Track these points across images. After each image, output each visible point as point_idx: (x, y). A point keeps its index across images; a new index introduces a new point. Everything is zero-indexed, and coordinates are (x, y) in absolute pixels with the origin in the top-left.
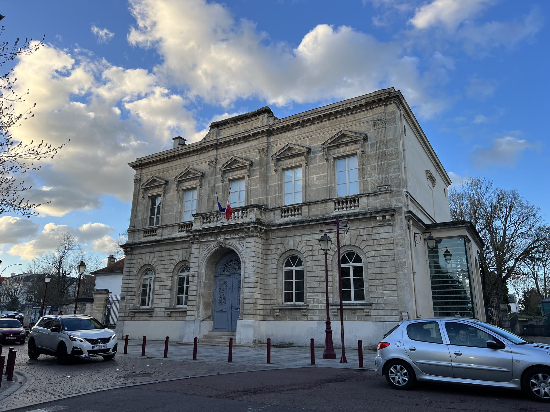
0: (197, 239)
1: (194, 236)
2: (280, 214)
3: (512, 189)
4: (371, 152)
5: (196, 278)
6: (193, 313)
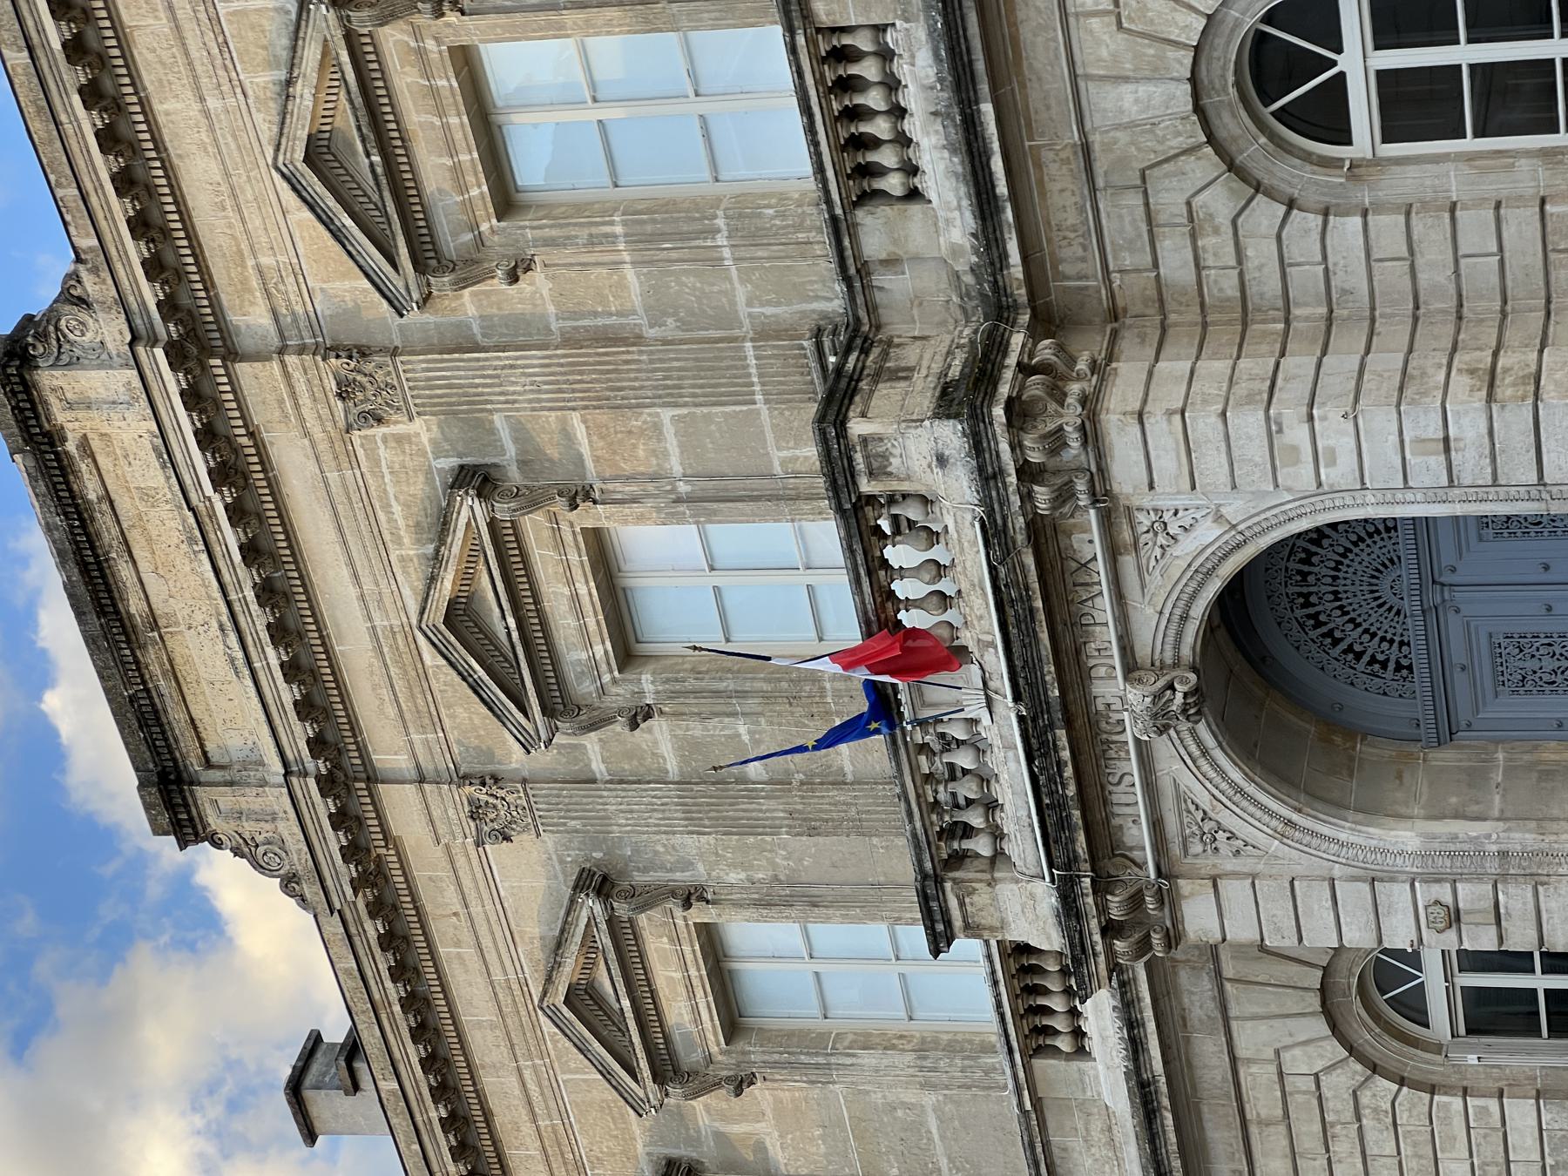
0: (1136, 901)
1: (1110, 930)
2: (885, 211)
3: (1095, 1054)
5: (1471, 895)
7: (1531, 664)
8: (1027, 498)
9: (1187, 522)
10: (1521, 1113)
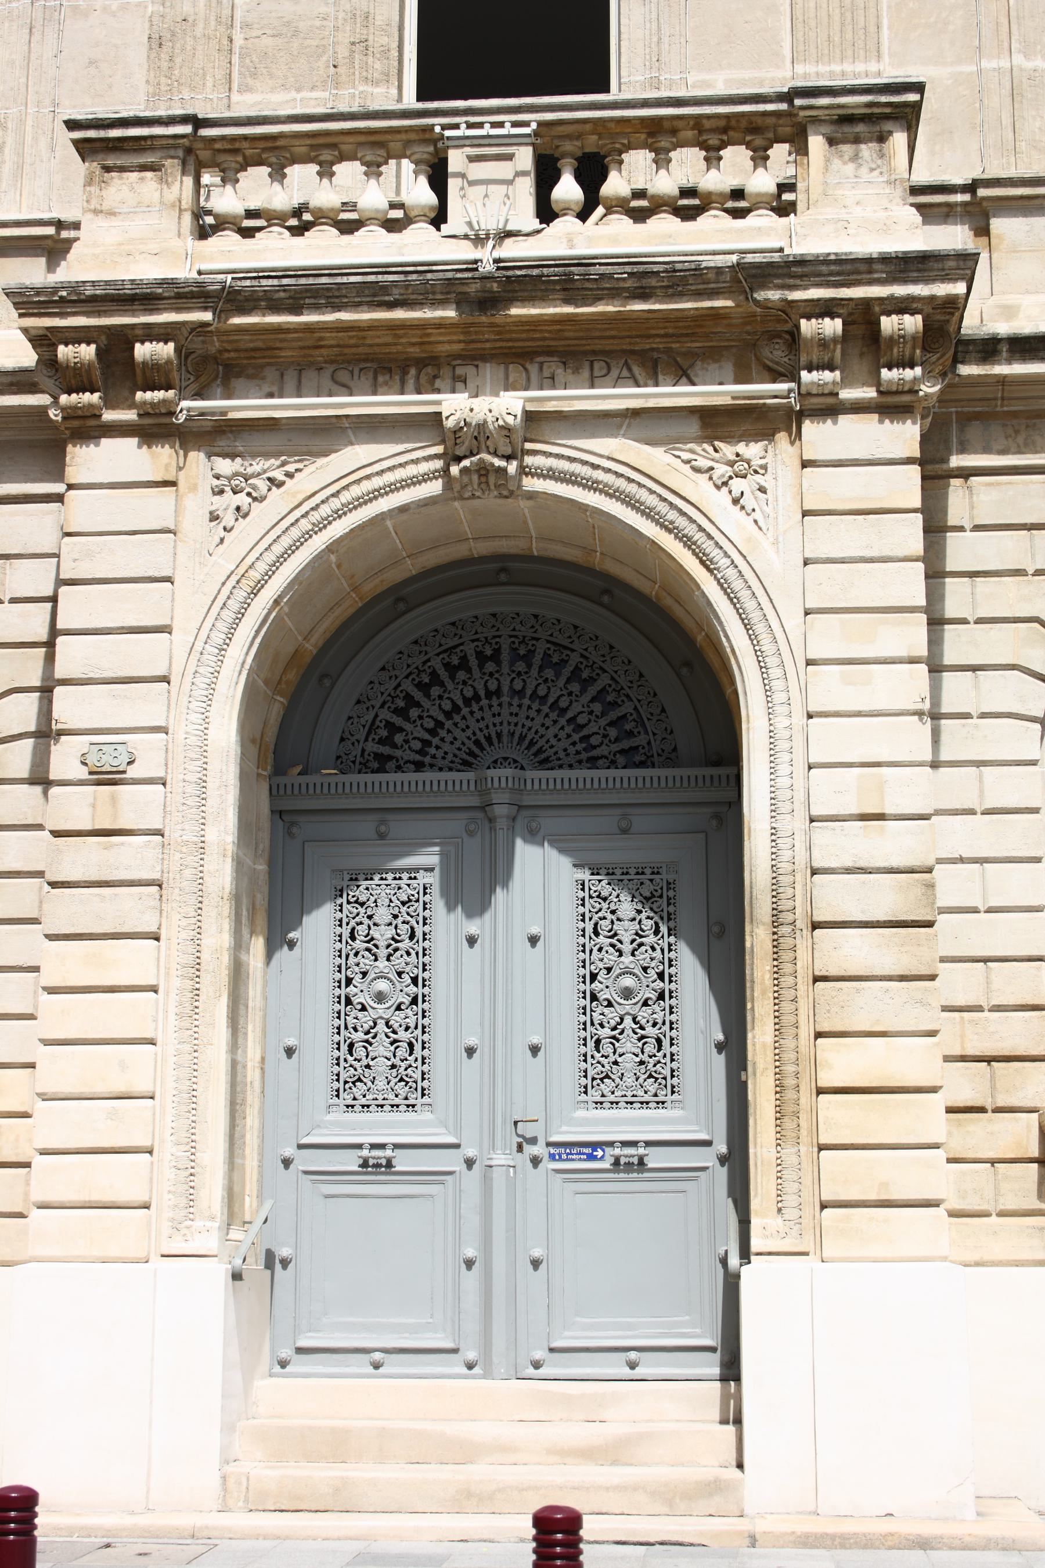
7: (383, 915)
8: (825, 309)
9: (748, 501)
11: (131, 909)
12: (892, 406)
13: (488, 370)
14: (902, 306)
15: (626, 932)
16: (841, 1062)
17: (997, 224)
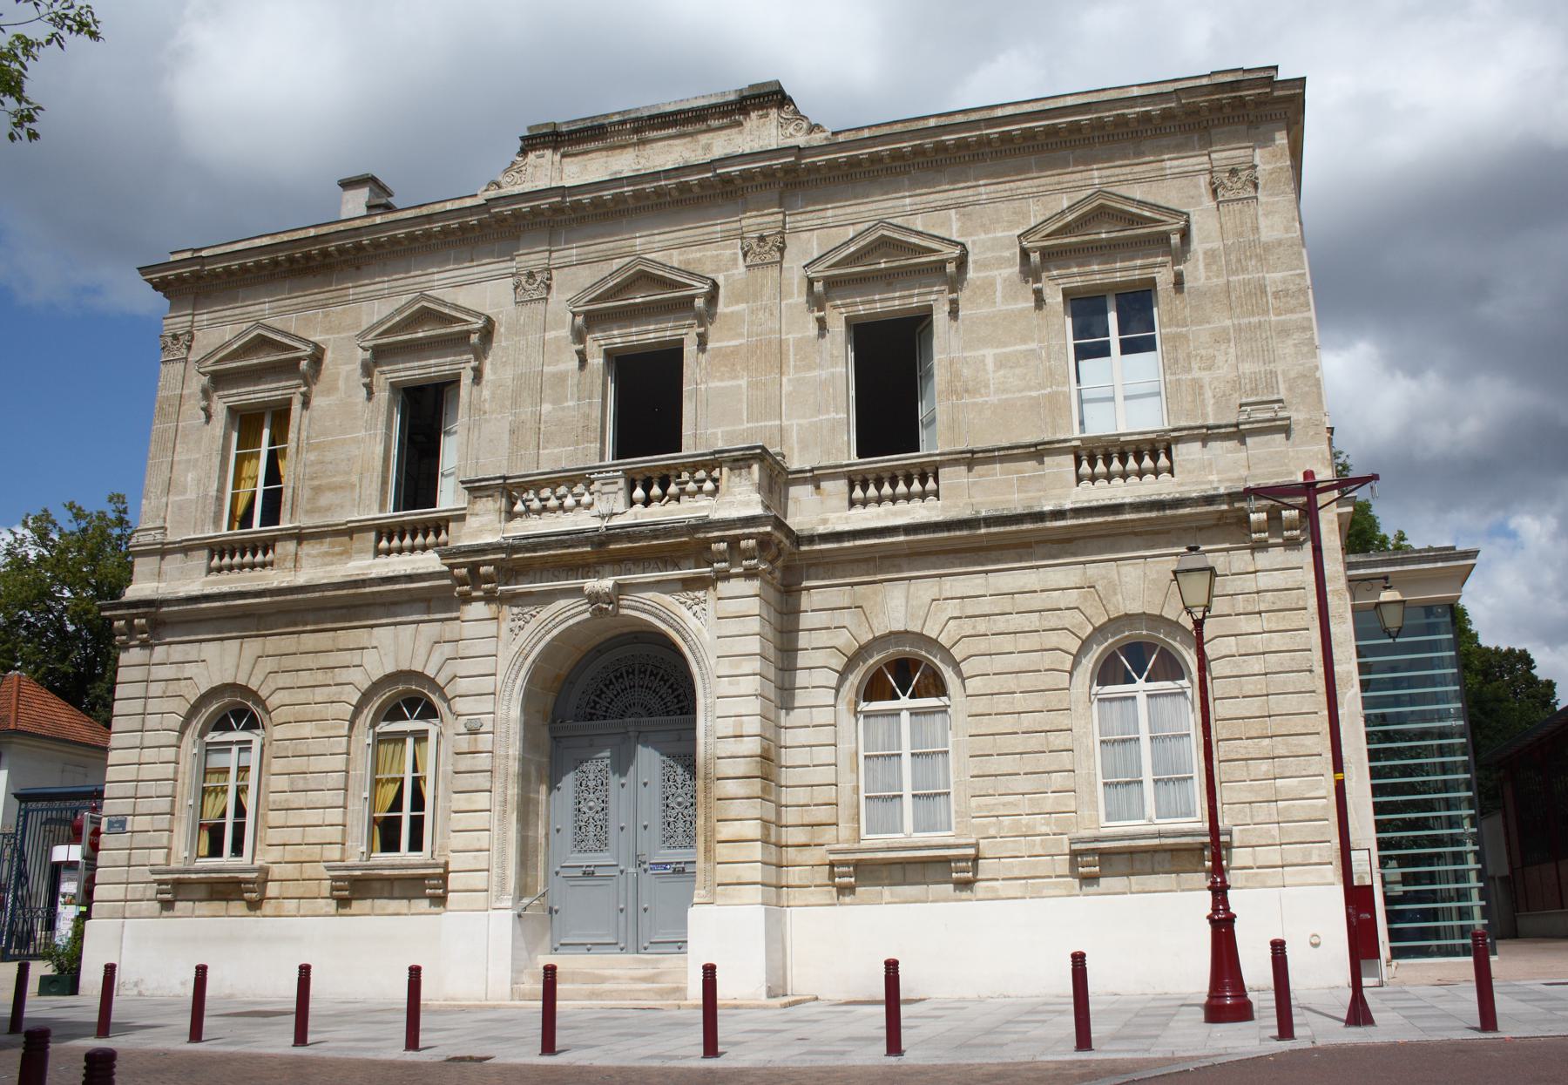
2: (846, 489)
3: (853, 511)
4: (1208, 278)
6: (478, 880)
7: (592, 776)
10: (339, 762)
11: (482, 781)
12: (750, 574)
13: (608, 568)
14: (749, 537)
15: (679, 779)
16: (726, 831)
17: (823, 484)
